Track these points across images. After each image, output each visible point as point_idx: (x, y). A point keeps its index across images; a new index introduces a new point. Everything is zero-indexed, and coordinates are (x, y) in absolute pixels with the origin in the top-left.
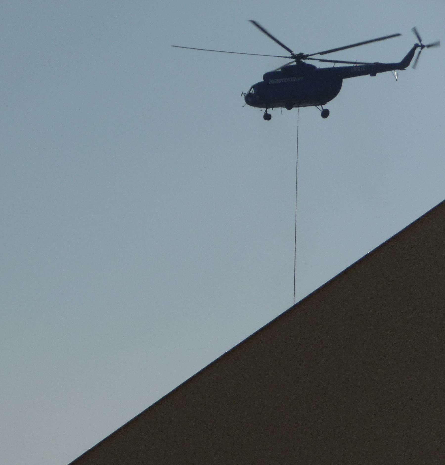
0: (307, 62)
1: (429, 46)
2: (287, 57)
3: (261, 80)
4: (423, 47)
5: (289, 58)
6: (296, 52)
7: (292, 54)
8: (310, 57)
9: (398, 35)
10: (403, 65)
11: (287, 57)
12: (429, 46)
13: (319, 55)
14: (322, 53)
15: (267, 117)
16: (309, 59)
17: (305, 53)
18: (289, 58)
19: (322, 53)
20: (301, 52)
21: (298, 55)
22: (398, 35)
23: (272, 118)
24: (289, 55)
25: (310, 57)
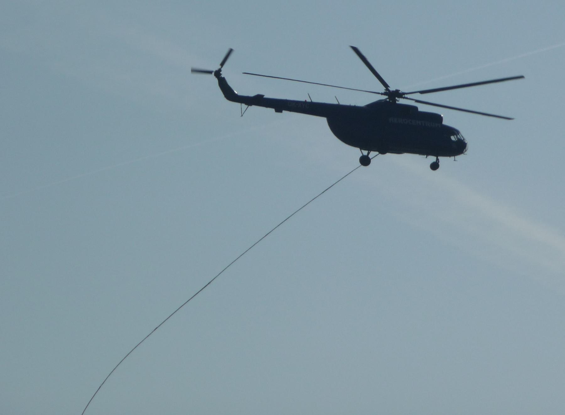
0: (401, 101)
1: (210, 72)
2: (379, 93)
3: (283, 111)
4: (220, 70)
5: (382, 94)
6: (392, 88)
7: (387, 89)
8: (406, 96)
9: (522, 77)
10: (229, 93)
11: (379, 93)
12: (210, 72)
13: (419, 94)
14: (422, 92)
15: (365, 161)
16: (405, 98)
17: (402, 90)
18: (382, 94)
19: (422, 92)
20: (398, 89)
21: (393, 91)
22: (522, 77)
23: (438, 170)
24: (382, 89)
25: (406, 96)
